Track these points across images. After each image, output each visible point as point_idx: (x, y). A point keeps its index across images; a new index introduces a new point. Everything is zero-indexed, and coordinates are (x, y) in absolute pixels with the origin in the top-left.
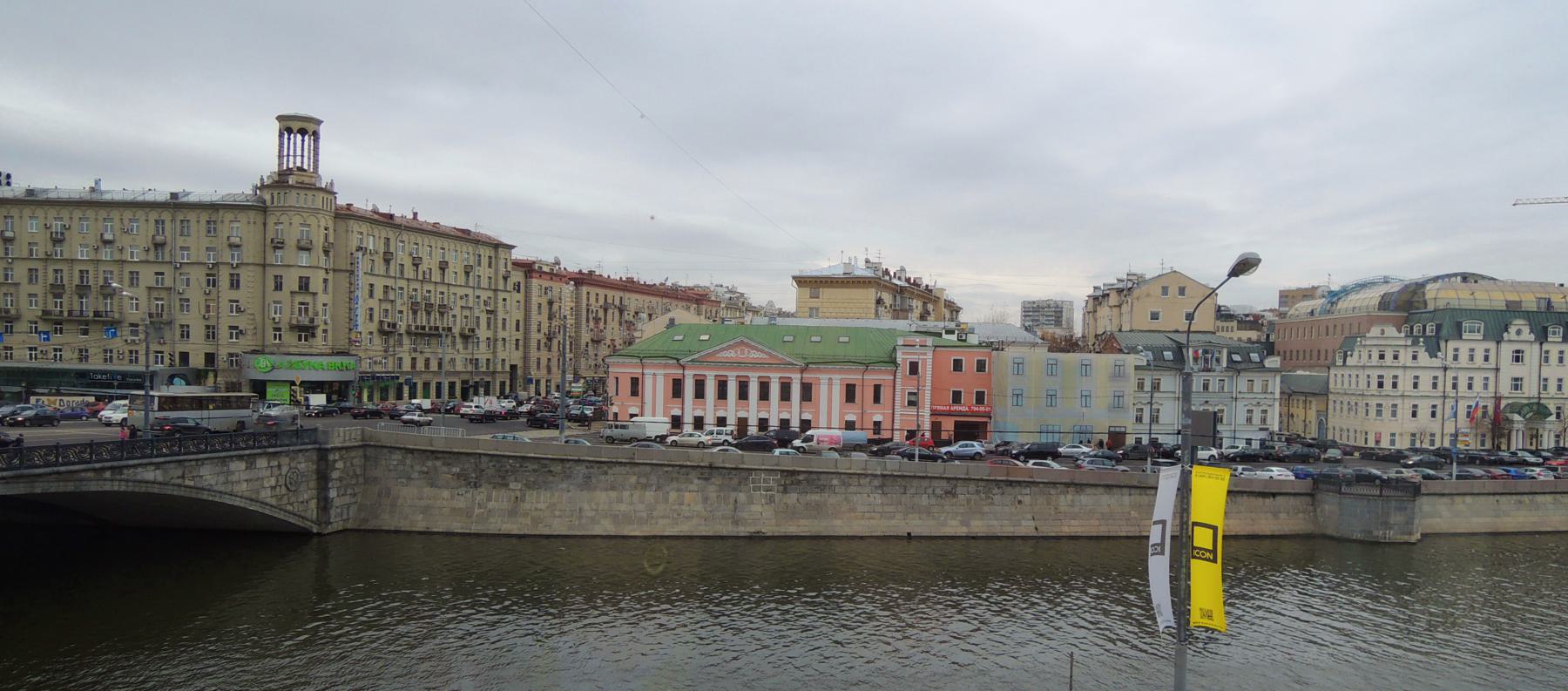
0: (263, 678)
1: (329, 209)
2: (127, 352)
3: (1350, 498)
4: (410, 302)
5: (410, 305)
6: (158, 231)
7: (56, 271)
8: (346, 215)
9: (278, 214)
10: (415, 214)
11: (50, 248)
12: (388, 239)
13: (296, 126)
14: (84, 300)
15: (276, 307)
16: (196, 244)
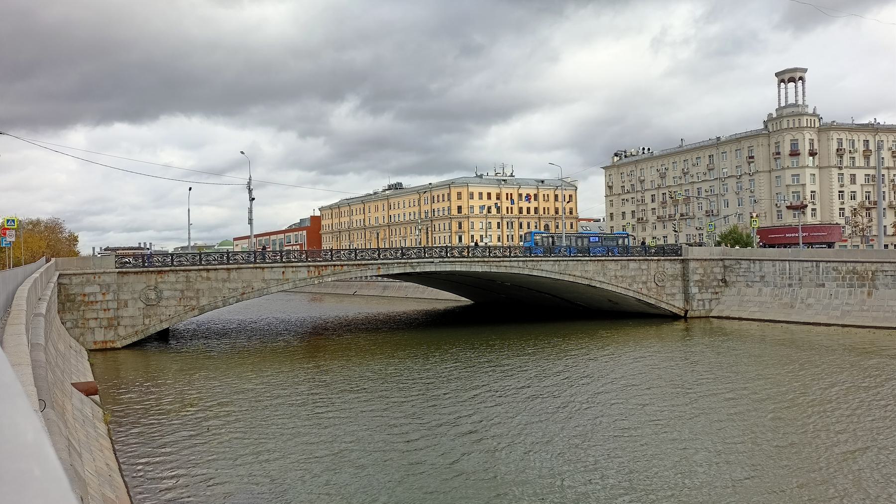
0: (189, 390)
1: (809, 126)
2: (698, 236)
3: (425, 302)
4: (891, 185)
5: (891, 187)
6: (710, 162)
7: (663, 194)
8: (825, 129)
9: (776, 136)
11: (660, 182)
12: (868, 141)
13: (786, 77)
14: (676, 208)
15: (866, 195)
16: (727, 164)
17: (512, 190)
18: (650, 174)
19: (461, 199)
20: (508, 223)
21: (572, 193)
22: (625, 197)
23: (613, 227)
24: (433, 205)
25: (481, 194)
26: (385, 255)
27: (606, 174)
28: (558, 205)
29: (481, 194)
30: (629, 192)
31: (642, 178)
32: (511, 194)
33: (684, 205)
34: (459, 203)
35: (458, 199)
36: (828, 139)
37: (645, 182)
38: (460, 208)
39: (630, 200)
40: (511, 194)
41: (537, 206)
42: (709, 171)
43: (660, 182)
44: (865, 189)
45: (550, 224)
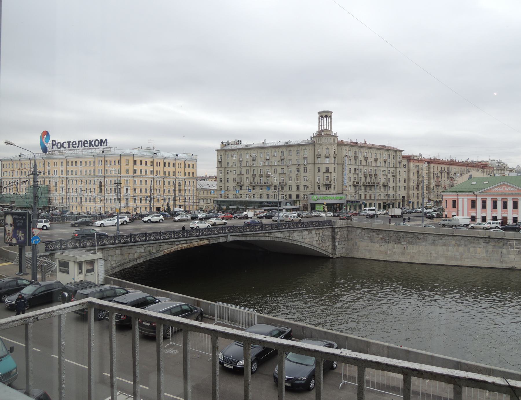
2: (273, 195)
7: (254, 170)
10: (365, 142)
11: (252, 163)
12: (356, 151)
13: (324, 115)
17: (181, 162)
18: (247, 157)
19: (128, 164)
20: (157, 181)
21: (194, 163)
22: (230, 169)
23: (221, 187)
24: (106, 166)
25: (141, 162)
26: (119, 241)
27: (217, 154)
28: (136, 167)
29: (141, 162)
30: (232, 167)
31: (241, 159)
32: (159, 162)
33: (259, 178)
34: (127, 167)
35: (126, 164)
36: (341, 150)
37: (243, 162)
38: (127, 171)
39: (233, 171)
40: (159, 162)
41: (174, 171)
42: (281, 161)
43: (252, 163)
44: (355, 176)
45: (181, 182)
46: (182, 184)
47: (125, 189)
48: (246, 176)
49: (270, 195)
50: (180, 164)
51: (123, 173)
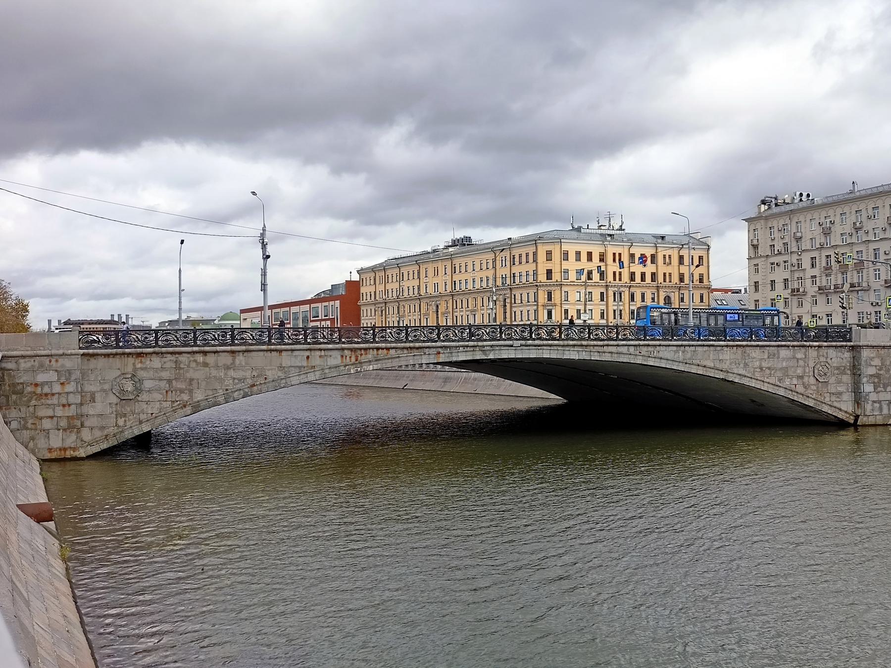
11: (823, 240)
20: (614, 294)
22: (775, 260)
25: (578, 254)
29: (578, 254)
30: (780, 253)
31: (799, 235)
32: (620, 254)
34: (549, 266)
35: (547, 260)
38: (549, 273)
39: (782, 264)
40: (620, 254)
43: (823, 240)
46: (672, 299)
47: (546, 312)
48: (810, 272)
49: (865, 313)
50: (667, 257)
51: (542, 277)
